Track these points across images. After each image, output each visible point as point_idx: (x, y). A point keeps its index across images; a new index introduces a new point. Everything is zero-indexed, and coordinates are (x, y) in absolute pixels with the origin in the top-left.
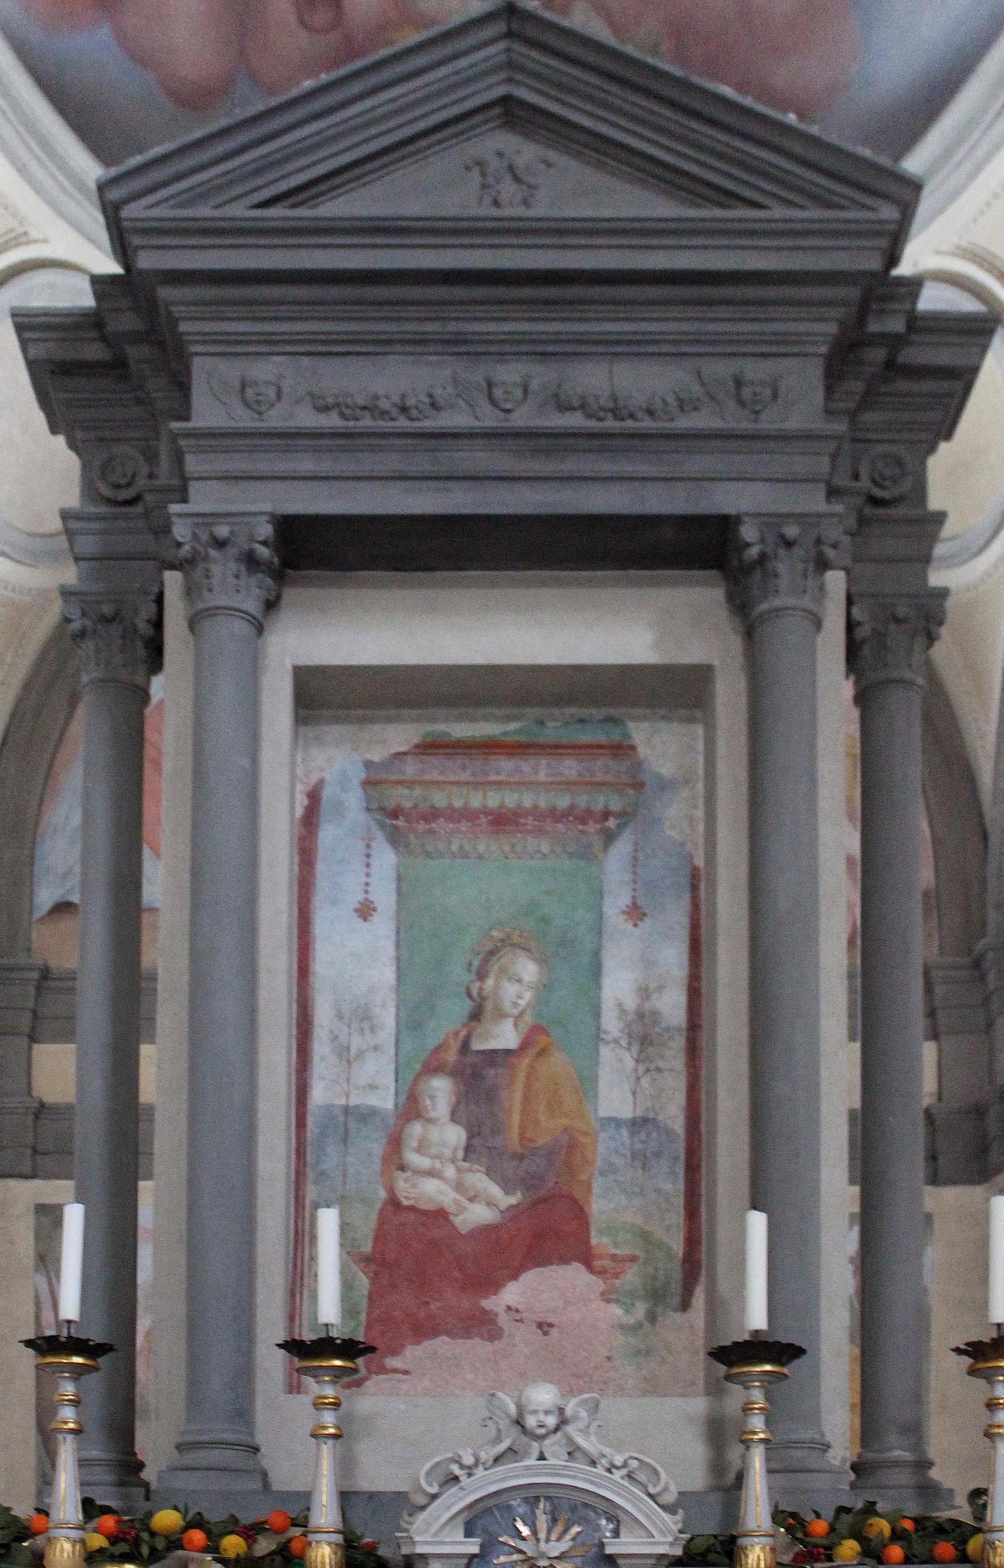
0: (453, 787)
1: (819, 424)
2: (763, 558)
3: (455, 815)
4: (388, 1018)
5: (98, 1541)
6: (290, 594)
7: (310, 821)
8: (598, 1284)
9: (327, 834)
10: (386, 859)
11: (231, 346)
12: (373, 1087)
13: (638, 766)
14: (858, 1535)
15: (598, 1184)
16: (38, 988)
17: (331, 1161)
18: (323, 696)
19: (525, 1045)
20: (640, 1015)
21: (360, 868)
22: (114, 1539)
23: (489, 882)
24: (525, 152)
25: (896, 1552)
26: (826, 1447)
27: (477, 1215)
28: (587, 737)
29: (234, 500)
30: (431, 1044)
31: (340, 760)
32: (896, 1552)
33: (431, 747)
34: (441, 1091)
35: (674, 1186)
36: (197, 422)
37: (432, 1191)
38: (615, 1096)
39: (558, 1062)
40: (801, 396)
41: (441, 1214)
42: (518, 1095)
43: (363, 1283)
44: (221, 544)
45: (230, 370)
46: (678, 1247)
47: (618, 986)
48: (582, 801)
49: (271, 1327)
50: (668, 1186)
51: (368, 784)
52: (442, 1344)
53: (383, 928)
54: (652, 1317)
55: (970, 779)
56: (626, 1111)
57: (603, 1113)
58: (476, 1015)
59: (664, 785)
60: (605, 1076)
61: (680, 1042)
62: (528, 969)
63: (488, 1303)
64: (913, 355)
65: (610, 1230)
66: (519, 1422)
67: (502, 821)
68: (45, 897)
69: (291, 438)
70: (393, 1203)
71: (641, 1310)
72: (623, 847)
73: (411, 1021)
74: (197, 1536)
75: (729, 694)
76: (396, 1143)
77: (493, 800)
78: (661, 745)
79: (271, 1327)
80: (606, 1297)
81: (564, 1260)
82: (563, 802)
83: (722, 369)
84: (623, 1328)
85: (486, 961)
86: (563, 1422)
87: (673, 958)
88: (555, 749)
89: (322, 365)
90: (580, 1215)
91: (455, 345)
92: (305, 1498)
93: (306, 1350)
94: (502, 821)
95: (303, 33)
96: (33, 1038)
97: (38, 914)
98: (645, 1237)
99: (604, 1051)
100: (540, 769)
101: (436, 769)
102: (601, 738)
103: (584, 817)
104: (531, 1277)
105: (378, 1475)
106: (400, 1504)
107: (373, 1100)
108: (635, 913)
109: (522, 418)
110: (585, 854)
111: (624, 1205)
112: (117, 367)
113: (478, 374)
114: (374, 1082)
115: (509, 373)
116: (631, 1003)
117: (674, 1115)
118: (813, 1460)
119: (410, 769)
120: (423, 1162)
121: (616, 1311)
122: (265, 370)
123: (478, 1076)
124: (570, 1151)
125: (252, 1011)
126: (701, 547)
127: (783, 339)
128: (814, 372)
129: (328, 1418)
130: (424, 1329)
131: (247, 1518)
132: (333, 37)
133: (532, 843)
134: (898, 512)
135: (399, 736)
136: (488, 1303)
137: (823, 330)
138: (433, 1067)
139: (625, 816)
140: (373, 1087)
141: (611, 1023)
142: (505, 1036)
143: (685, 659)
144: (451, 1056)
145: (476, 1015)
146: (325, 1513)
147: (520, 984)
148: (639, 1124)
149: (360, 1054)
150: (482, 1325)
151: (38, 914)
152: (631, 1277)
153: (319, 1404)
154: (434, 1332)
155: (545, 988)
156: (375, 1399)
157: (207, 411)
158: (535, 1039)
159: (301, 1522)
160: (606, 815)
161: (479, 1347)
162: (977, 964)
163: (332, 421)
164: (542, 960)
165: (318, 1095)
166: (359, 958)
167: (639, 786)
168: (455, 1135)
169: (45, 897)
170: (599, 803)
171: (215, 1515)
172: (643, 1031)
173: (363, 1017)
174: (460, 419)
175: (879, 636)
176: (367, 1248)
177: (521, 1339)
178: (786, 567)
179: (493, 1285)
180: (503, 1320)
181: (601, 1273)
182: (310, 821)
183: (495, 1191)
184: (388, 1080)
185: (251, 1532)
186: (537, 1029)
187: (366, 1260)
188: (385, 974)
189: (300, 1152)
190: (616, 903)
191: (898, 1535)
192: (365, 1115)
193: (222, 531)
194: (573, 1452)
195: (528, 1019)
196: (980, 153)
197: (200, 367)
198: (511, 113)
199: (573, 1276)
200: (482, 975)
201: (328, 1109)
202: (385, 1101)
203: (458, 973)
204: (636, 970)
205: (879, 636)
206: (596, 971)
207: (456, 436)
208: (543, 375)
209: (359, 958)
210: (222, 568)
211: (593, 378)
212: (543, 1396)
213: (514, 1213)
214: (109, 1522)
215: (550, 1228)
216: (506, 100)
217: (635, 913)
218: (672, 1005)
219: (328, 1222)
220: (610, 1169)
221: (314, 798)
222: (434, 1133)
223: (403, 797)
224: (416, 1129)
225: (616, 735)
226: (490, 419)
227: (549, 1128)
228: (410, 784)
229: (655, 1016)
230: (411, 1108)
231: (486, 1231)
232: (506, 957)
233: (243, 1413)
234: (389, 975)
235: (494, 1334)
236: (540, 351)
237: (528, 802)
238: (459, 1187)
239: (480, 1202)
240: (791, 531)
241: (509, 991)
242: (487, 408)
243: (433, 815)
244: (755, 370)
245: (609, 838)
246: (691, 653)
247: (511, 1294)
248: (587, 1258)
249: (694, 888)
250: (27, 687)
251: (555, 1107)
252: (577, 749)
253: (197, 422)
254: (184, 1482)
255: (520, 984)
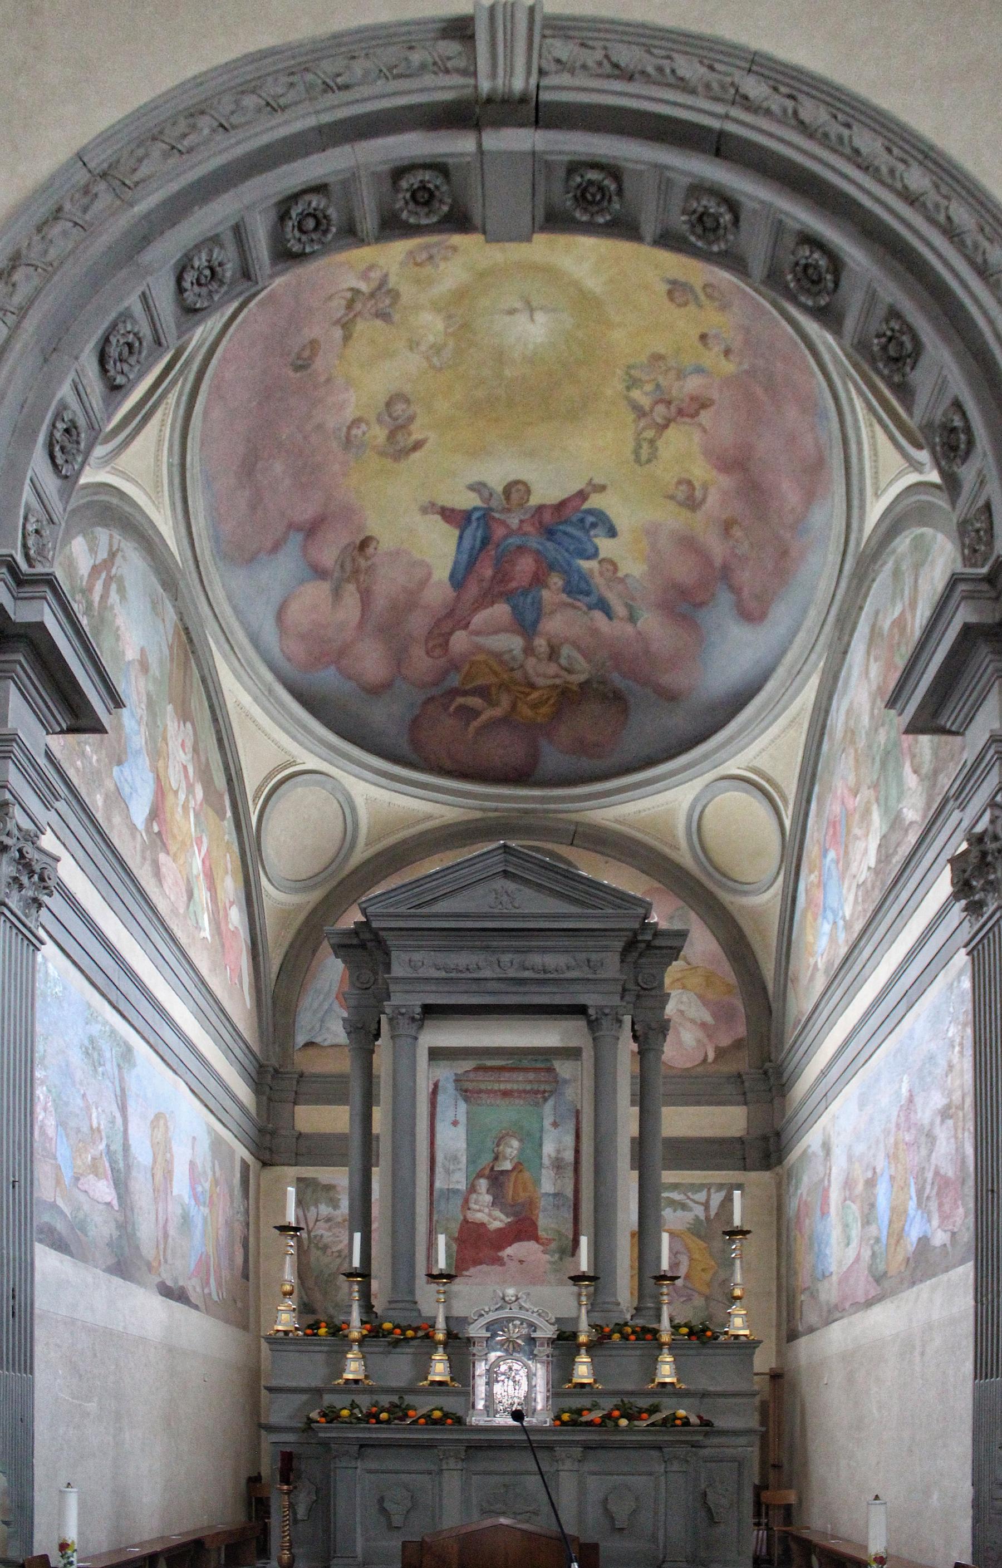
0: (488, 1082)
1: (617, 976)
2: (597, 1019)
3: (489, 1092)
4: (464, 1159)
5: (365, 1332)
6: (426, 1022)
7: (435, 1092)
8: (541, 1248)
9: (440, 1098)
10: (463, 1107)
11: (404, 948)
12: (458, 1182)
13: (557, 1075)
14: (620, 1332)
15: (541, 1215)
16: (298, 1082)
17: (443, 1205)
18: (436, 1054)
19: (514, 1169)
20: (557, 1159)
21: (453, 1110)
22: (370, 1331)
23: (502, 1114)
24: (511, 886)
25: (633, 1337)
26: (619, 1304)
27: (496, 1225)
28: (539, 1065)
29: (407, 1000)
30: (480, 1167)
31: (445, 1073)
32: (633, 1337)
33: (477, 1069)
34: (483, 1184)
35: (570, 1216)
36: (393, 974)
37: (480, 1217)
38: (548, 1184)
39: (526, 1175)
40: (611, 965)
41: (483, 1225)
42: (511, 1184)
43: (455, 1247)
44: (403, 1014)
45: (405, 956)
46: (571, 1237)
47: (549, 1149)
48: (535, 1087)
49: (421, 1270)
50: (566, 1216)
51: (456, 1081)
52: (484, 1267)
53: (461, 1130)
54: (561, 1259)
55: (764, 989)
56: (552, 1191)
57: (543, 1191)
58: (496, 1158)
59: (566, 1082)
60: (543, 1180)
61: (571, 1168)
62: (515, 1144)
63: (500, 1254)
64: (657, 943)
65: (545, 1230)
66: (503, 1298)
67: (506, 1094)
68: (301, 1039)
69: (427, 980)
70: (466, 1221)
71: (557, 1256)
72: (550, 1103)
73: (472, 1160)
74: (398, 1331)
75: (588, 1054)
76: (466, 1201)
77: (502, 1087)
78: (564, 1069)
79: (421, 1270)
80: (544, 1252)
81: (529, 1239)
82: (528, 1087)
83: (583, 956)
84: (550, 1262)
85: (500, 1141)
86: (517, 1299)
87: (569, 1140)
88: (526, 1070)
89: (438, 954)
90: (534, 1225)
91: (487, 948)
92: (434, 1318)
93: (432, 1277)
94: (506, 1094)
95: (430, 660)
96: (295, 1103)
97: (297, 1047)
98: (558, 1232)
99: (544, 1171)
100: (521, 1076)
101: (481, 1075)
102: (543, 1066)
103: (537, 1092)
104: (516, 1245)
105: (459, 1310)
106: (464, 1321)
107: (459, 1187)
108: (555, 1125)
109: (512, 973)
110: (537, 1104)
111: (549, 1221)
112: (363, 946)
113: (493, 959)
114: (459, 1181)
115: (506, 958)
116: (553, 1155)
117: (569, 1192)
118: (615, 1308)
119: (472, 1075)
120: (477, 1207)
121: (547, 1257)
122: (417, 956)
123: (497, 1179)
124: (531, 1204)
125: (414, 1159)
126: (579, 1010)
127: (606, 947)
128: (617, 957)
129: (442, 1296)
130: (477, 1262)
131: (414, 1325)
132: (443, 660)
133: (517, 1101)
134: (653, 993)
135: (468, 1065)
136: (500, 1254)
137: (619, 945)
138: (480, 1175)
139: (552, 1093)
140: (458, 1182)
141: (546, 1161)
142: (507, 1166)
143: (571, 1045)
144: (487, 1172)
145: (496, 1158)
146: (441, 1324)
147: (513, 1147)
148: (556, 1195)
149: (453, 1171)
150: (499, 1261)
151: (297, 1047)
152: (553, 1245)
153: (438, 1292)
154: (481, 1263)
155: (521, 1151)
156: (458, 1286)
157: (398, 970)
158: (518, 1167)
159: (433, 1326)
160: (545, 1092)
161: (497, 1268)
162: (765, 1073)
163: (443, 974)
164: (521, 1141)
165: (438, 1185)
166: (453, 1138)
167: (557, 1082)
168: (488, 1198)
169: (301, 1039)
170: (542, 1088)
171: (403, 1323)
172: (558, 1165)
173: (455, 1159)
174: (487, 973)
175: (646, 1034)
176: (456, 1235)
177: (512, 1266)
178: (605, 1023)
179: (502, 1248)
180: (506, 1259)
181: (542, 1244)
182: (435, 1092)
183: (503, 1217)
184: (464, 1180)
185: (416, 1330)
186: (519, 1163)
187: (456, 1240)
188: (462, 1145)
189: (431, 1203)
190: (547, 1122)
191: (633, 1332)
192: (456, 1192)
193: (403, 1010)
194: (521, 1308)
195: (516, 1160)
196: (755, 733)
197: (394, 954)
198: (506, 874)
199: (532, 1245)
200: (498, 1145)
201: (441, 1190)
202: (462, 1187)
203: (489, 1144)
204: (556, 1142)
205: (646, 1034)
206: (541, 1145)
207: (486, 979)
208: (518, 958)
209: (453, 1138)
210: (403, 1021)
211: (536, 959)
212: (511, 1292)
213: (509, 1224)
214: (368, 1326)
215: (523, 1228)
216: (505, 872)
217: (555, 1125)
218: (569, 1156)
219: (442, 1240)
220: (545, 1210)
221: (436, 1086)
222: (481, 1198)
223: (470, 1086)
224: (474, 1196)
225: (548, 1065)
226: (499, 973)
227: (523, 1197)
228: (472, 1081)
229: (562, 1159)
230: (472, 1189)
231: (499, 1230)
232: (507, 1138)
233: (412, 1292)
234: (464, 1146)
235: (503, 1264)
236: (517, 951)
237: (515, 1087)
238: (490, 1215)
239: (497, 1220)
240: (607, 1011)
241: (509, 1150)
242: (498, 970)
243: (480, 1091)
244: (594, 957)
245: (545, 1100)
246: (573, 1043)
247: (509, 1251)
248: (537, 1239)
249: (577, 1118)
250: (291, 946)
251: (525, 1189)
252: (535, 1070)
253: (393, 974)
254: (391, 1313)
255: (513, 1147)
